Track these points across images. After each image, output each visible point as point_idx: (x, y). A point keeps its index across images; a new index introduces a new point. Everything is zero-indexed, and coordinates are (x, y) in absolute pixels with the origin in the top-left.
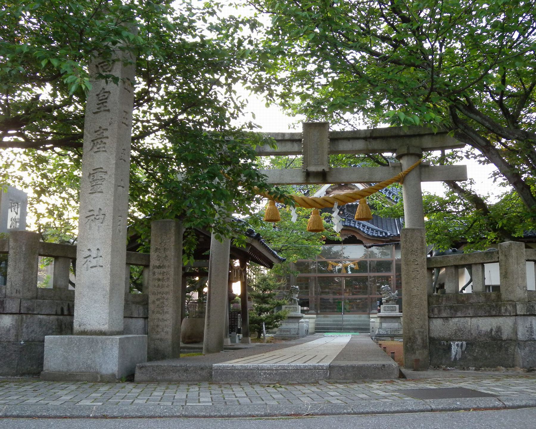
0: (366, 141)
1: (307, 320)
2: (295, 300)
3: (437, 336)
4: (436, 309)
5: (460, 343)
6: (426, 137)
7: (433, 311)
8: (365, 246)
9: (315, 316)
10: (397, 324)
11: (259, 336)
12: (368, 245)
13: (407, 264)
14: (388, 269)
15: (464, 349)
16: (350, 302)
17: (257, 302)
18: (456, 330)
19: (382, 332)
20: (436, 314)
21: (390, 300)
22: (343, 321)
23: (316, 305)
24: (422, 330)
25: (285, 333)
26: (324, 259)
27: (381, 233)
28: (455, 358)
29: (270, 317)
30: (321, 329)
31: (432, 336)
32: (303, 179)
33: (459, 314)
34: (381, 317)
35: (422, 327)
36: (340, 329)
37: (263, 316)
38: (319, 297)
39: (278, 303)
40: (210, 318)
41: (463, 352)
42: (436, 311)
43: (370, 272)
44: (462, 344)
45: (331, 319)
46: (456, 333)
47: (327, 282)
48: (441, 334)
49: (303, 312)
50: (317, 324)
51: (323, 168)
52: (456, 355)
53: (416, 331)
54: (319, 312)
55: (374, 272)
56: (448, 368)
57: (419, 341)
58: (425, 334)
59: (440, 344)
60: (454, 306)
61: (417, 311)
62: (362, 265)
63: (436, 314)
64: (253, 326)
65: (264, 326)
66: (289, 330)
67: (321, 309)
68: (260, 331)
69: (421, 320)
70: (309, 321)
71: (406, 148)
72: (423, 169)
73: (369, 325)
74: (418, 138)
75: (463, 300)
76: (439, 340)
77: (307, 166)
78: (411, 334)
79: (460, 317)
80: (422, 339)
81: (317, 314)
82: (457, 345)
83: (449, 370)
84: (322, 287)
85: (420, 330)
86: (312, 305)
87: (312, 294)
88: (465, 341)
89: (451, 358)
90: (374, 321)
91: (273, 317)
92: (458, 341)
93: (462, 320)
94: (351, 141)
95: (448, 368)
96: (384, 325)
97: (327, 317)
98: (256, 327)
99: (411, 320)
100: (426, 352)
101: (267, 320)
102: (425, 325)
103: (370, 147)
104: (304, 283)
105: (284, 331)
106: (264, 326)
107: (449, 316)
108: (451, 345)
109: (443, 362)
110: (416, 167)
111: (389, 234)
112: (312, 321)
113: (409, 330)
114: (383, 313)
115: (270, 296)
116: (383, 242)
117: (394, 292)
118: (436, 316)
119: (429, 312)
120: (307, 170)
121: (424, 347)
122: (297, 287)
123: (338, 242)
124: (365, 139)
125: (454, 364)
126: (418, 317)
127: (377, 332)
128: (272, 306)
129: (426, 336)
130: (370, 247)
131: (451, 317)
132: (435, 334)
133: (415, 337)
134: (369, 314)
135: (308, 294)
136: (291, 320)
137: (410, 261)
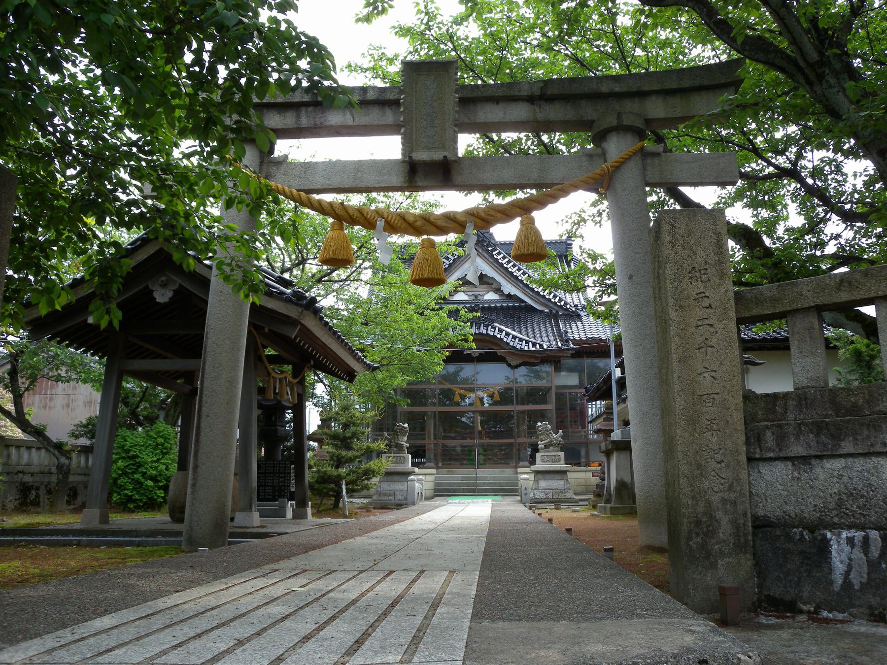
0: (533, 104)
1: (421, 477)
2: (402, 446)
3: (778, 512)
4: (769, 434)
5: (859, 535)
6: (654, 98)
7: (759, 439)
8: (509, 365)
9: (434, 471)
10: (562, 482)
11: (336, 505)
12: (514, 363)
13: (681, 306)
14: (544, 401)
15: (875, 552)
16: (485, 450)
17: (335, 446)
18: (839, 493)
19: (539, 495)
20: (769, 450)
21: (551, 445)
22: (476, 478)
23: (435, 455)
24: (732, 496)
25: (386, 498)
26: (447, 386)
27: (534, 344)
28: (847, 584)
29: (354, 472)
30: (442, 492)
31: (761, 513)
32: (402, 179)
33: (848, 446)
34: (537, 472)
35: (731, 488)
36: (474, 490)
37: (343, 471)
38: (441, 441)
39: (368, 447)
40: (199, 470)
41: (873, 565)
42: (769, 438)
43: (517, 404)
44: (866, 540)
45: (458, 475)
46: (840, 504)
47: (450, 422)
48: (789, 508)
49: (414, 464)
50: (436, 484)
51: (445, 154)
52: (847, 573)
53: (715, 499)
54: (440, 465)
55: (523, 404)
56: (825, 614)
57: (725, 529)
58: (741, 508)
59: (789, 538)
60: (827, 424)
61: (715, 439)
62: (505, 396)
63: (769, 450)
64: (325, 488)
65: (344, 487)
66: (392, 493)
67: (443, 460)
68: (338, 496)
69: (728, 466)
70: (423, 479)
71: (615, 116)
72: (649, 161)
73: (517, 484)
74: (637, 100)
75: (855, 405)
76: (784, 524)
77: (411, 152)
78: (701, 509)
79: (852, 455)
80: (734, 522)
81: (437, 468)
82: (850, 541)
83: (827, 621)
84: (445, 431)
85: (726, 495)
86: (430, 454)
87: (429, 437)
88: (878, 528)
89: (831, 583)
90: (525, 476)
91: (360, 471)
92: (849, 527)
93: (859, 464)
94: (501, 105)
95: (825, 614)
96: (543, 484)
97: (452, 473)
98: (332, 490)
99: (699, 467)
100: (746, 562)
101: (350, 478)
102: (738, 480)
103: (540, 116)
104: (417, 423)
105: (385, 495)
106: (344, 487)
107: (813, 453)
108: (826, 542)
109: (805, 594)
110: (635, 154)
111: (545, 347)
112: (431, 478)
113: (693, 498)
114: (539, 466)
115: (354, 435)
116: (536, 358)
117: (556, 433)
118: (771, 455)
119: (748, 443)
120: (410, 157)
121: (740, 547)
122: (406, 425)
123: (469, 359)
124: (531, 99)
125: (845, 599)
126: (719, 457)
127: (531, 496)
128: (358, 454)
129: (745, 514)
130: (517, 367)
131: (820, 457)
132: (770, 508)
133: (712, 517)
134: (516, 467)
135: (424, 439)
136: (396, 478)
137: (688, 297)
